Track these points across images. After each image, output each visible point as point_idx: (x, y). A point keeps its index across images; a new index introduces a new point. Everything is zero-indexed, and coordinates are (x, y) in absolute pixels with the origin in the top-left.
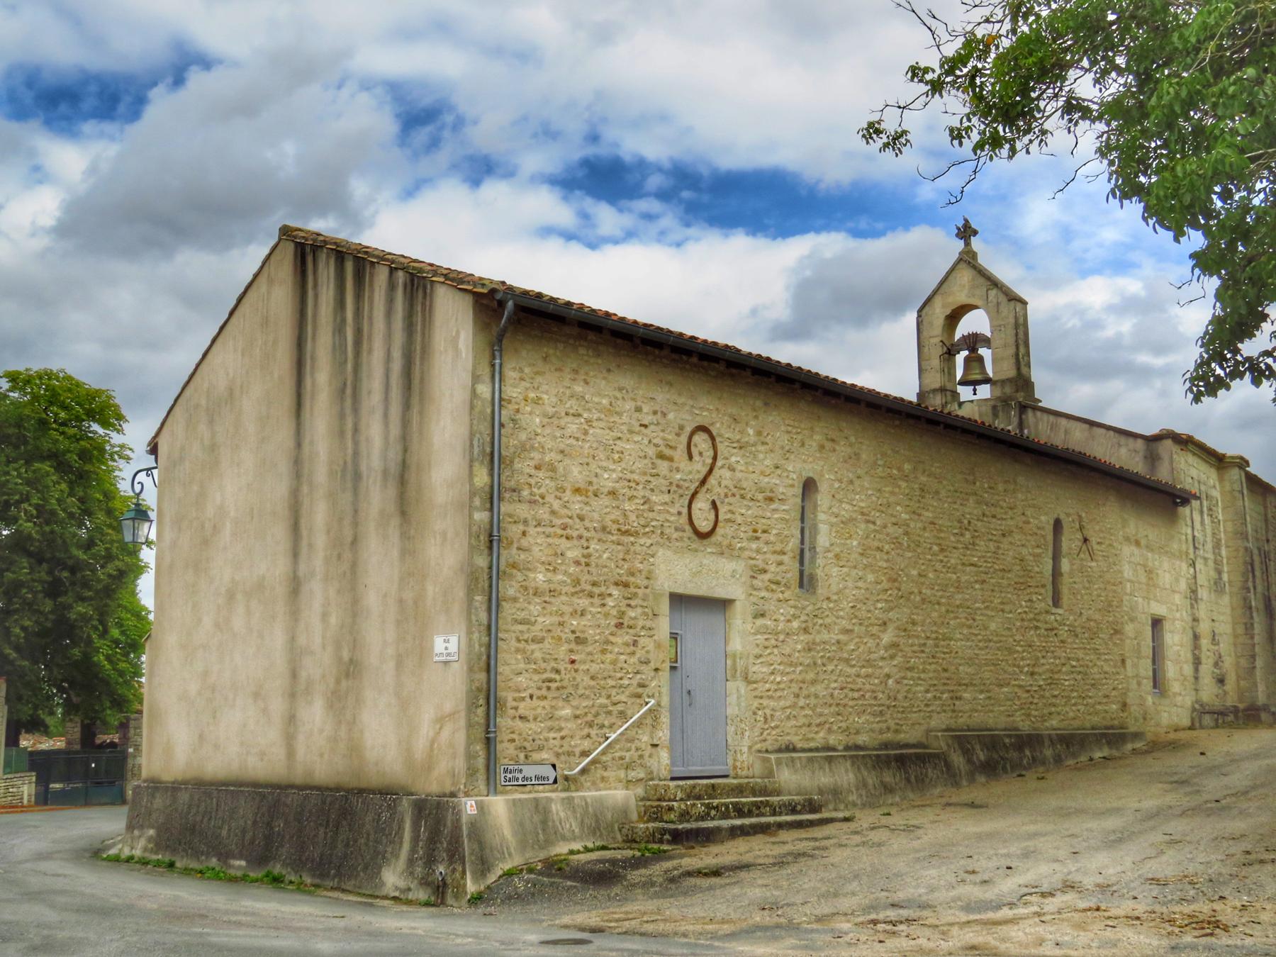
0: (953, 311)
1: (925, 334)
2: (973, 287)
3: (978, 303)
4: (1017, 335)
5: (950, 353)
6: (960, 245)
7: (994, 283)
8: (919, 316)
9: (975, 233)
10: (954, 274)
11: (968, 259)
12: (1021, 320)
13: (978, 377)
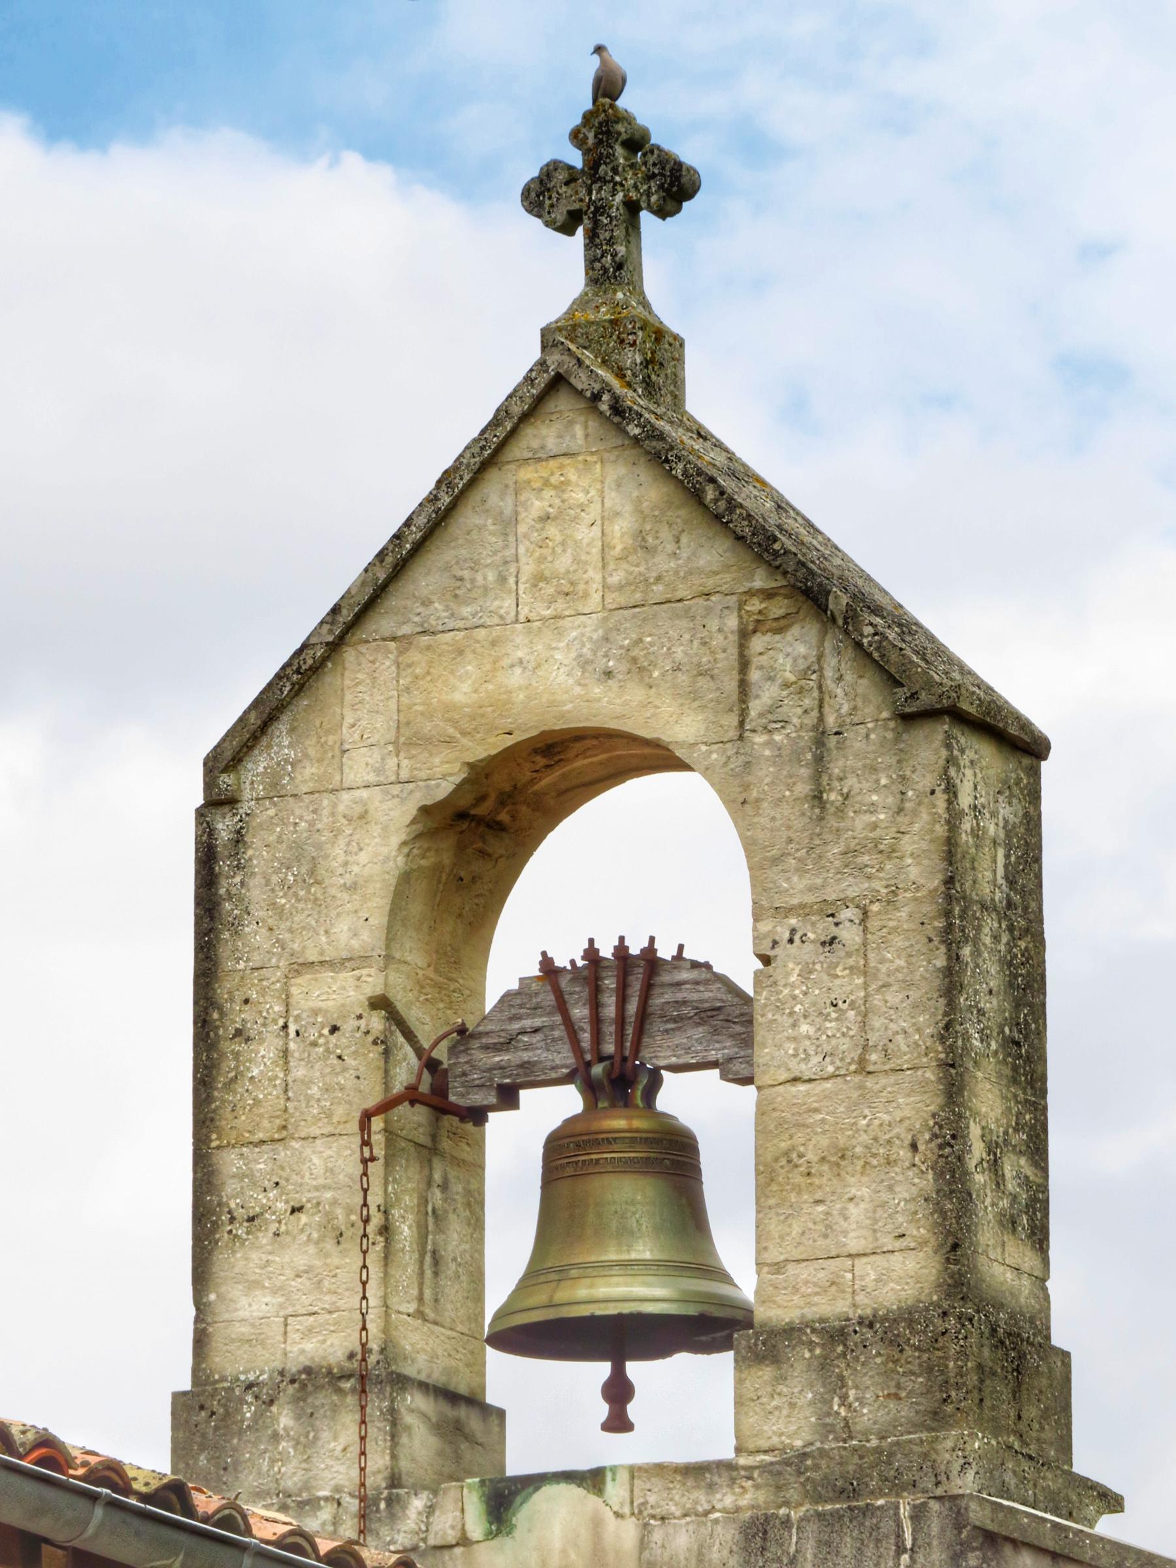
0: (480, 774)
1: (252, 944)
2: (641, 603)
3: (680, 726)
4: (951, 982)
5: (438, 1107)
6: (553, 271)
7: (803, 582)
8: (217, 801)
9: (674, 187)
10: (230, 964)
11: (609, 376)
12: (988, 876)
13: (652, 1295)
